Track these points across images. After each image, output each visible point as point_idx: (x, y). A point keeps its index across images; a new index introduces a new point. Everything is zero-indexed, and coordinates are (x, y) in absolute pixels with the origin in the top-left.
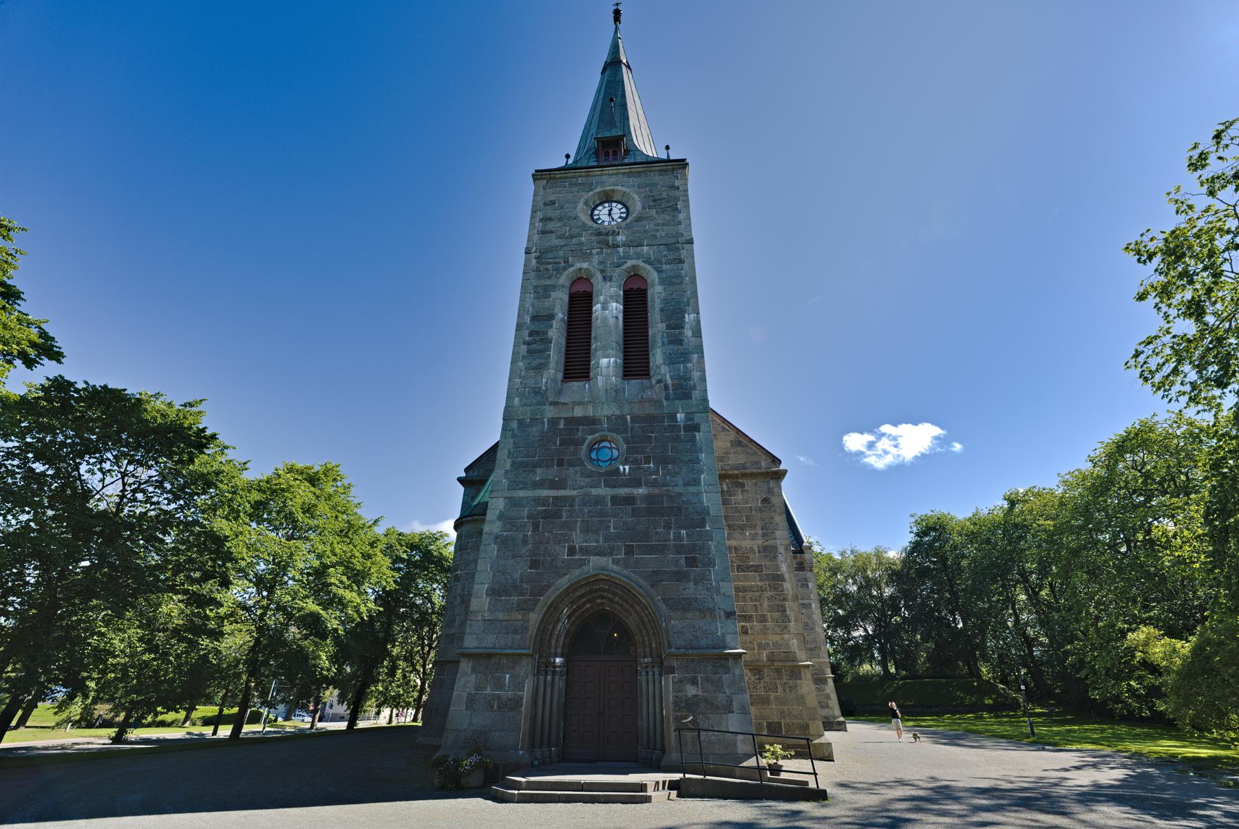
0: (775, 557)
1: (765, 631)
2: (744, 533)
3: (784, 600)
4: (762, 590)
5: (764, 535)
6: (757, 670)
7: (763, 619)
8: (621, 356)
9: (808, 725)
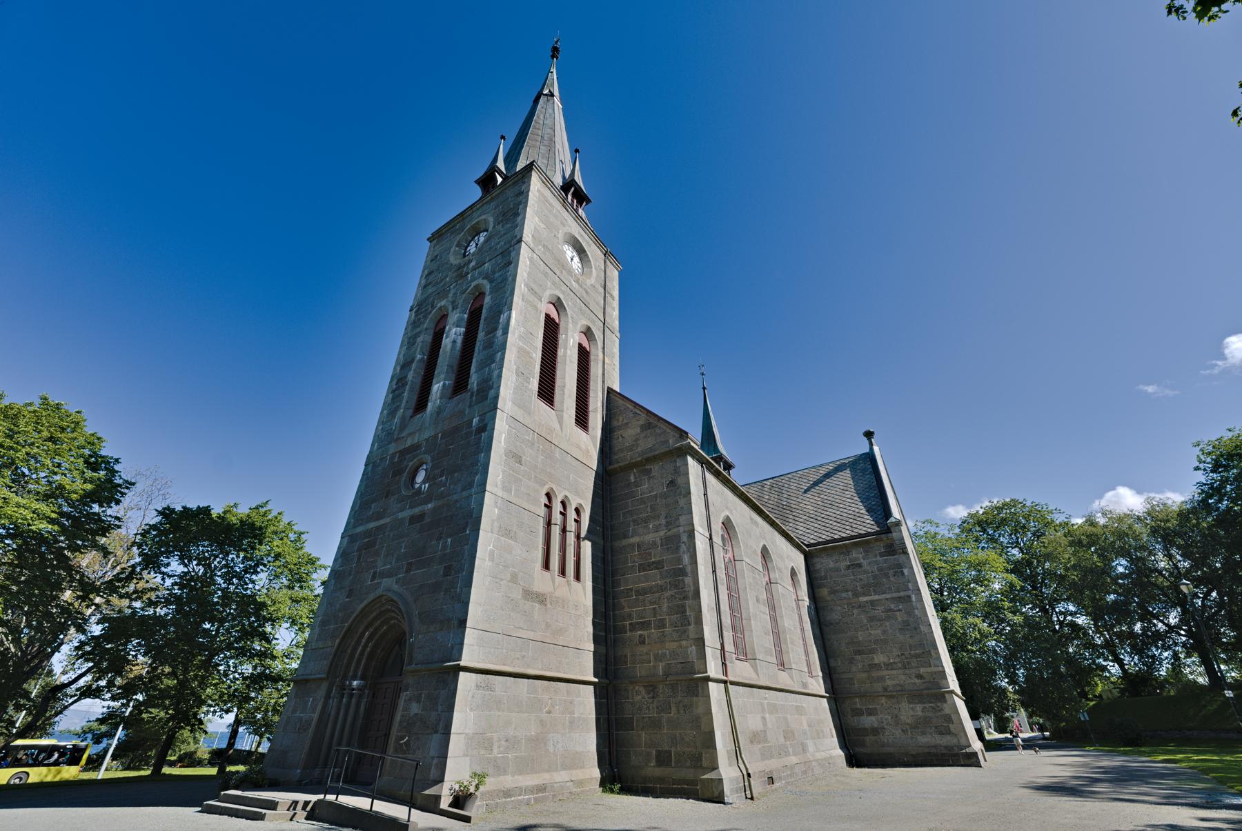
0: (678, 548)
1: (662, 639)
2: (647, 527)
3: (685, 598)
4: (662, 589)
5: (668, 524)
6: (652, 688)
7: (661, 624)
8: (453, 377)
9: (701, 755)
